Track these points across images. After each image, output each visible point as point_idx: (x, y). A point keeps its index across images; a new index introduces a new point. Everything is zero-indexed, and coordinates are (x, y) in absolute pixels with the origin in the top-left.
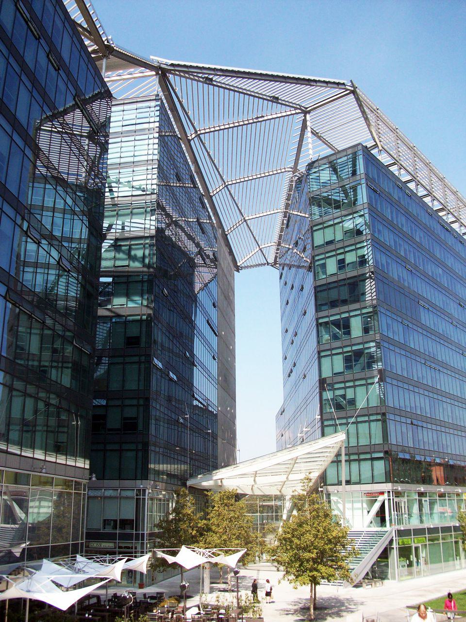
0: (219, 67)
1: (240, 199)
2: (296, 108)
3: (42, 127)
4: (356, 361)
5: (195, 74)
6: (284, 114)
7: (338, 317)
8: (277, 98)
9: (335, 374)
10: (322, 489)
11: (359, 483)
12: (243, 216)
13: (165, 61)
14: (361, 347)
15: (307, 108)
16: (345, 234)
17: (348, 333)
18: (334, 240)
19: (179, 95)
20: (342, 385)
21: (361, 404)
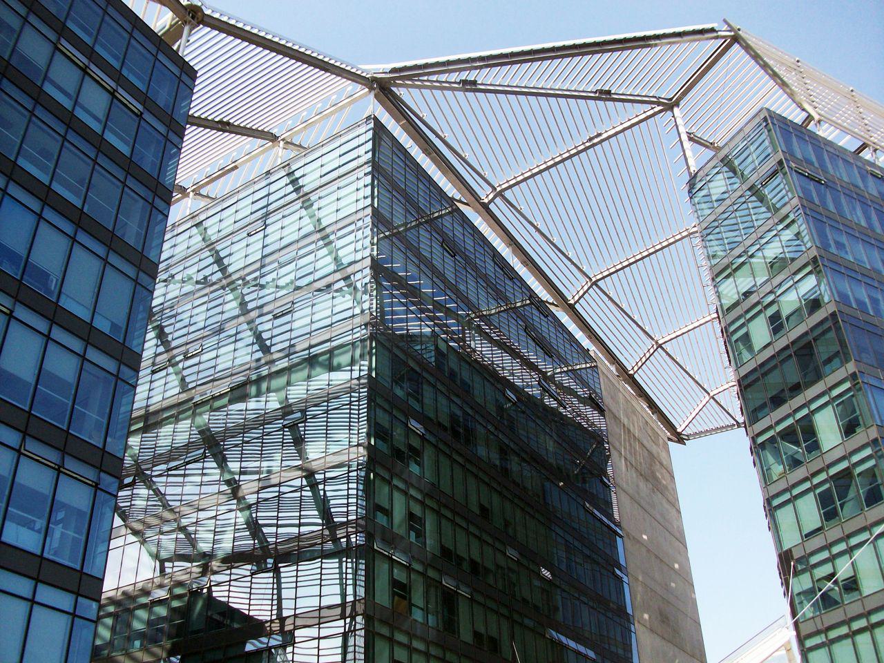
1: (632, 304)
7: (790, 421)
9: (806, 536)
12: (653, 339)
13: (378, 67)
15: (671, 99)
16: (771, 267)
17: (814, 446)
19: (467, 155)
20: (825, 555)
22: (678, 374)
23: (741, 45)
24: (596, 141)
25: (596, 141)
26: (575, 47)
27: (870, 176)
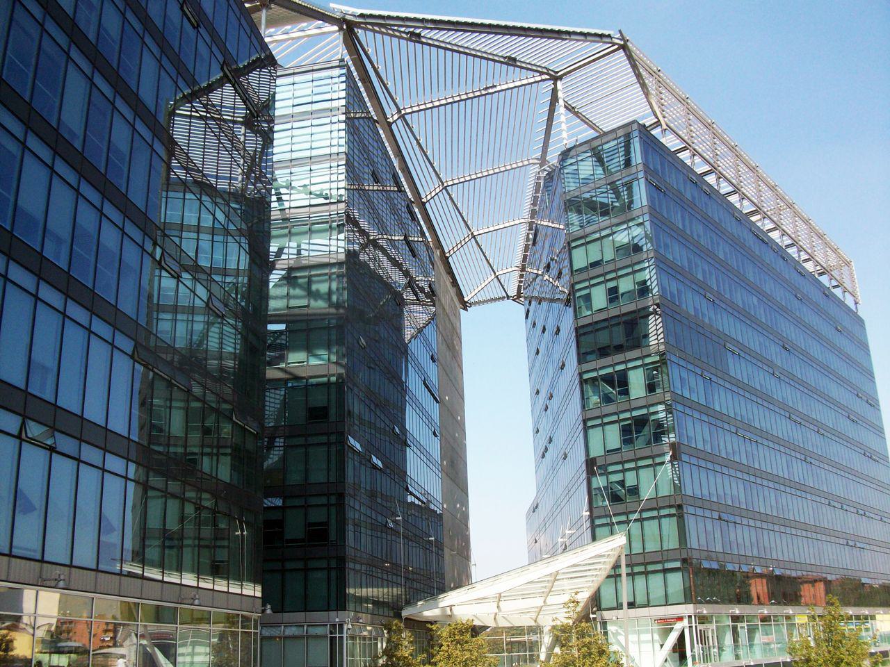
0: (429, 17)
2: (542, 73)
3: (178, 112)
4: (638, 432)
5: (396, 28)
6: (525, 82)
7: (610, 370)
8: (514, 60)
9: (608, 451)
10: (594, 616)
11: (647, 605)
13: (351, 10)
14: (644, 411)
15: (557, 72)
16: (617, 251)
17: (626, 392)
18: (602, 260)
20: (619, 467)
21: (647, 493)
22: (478, 255)
23: (626, 54)
24: (490, 91)
25: (490, 91)
26: (506, 27)
27: (689, 182)
